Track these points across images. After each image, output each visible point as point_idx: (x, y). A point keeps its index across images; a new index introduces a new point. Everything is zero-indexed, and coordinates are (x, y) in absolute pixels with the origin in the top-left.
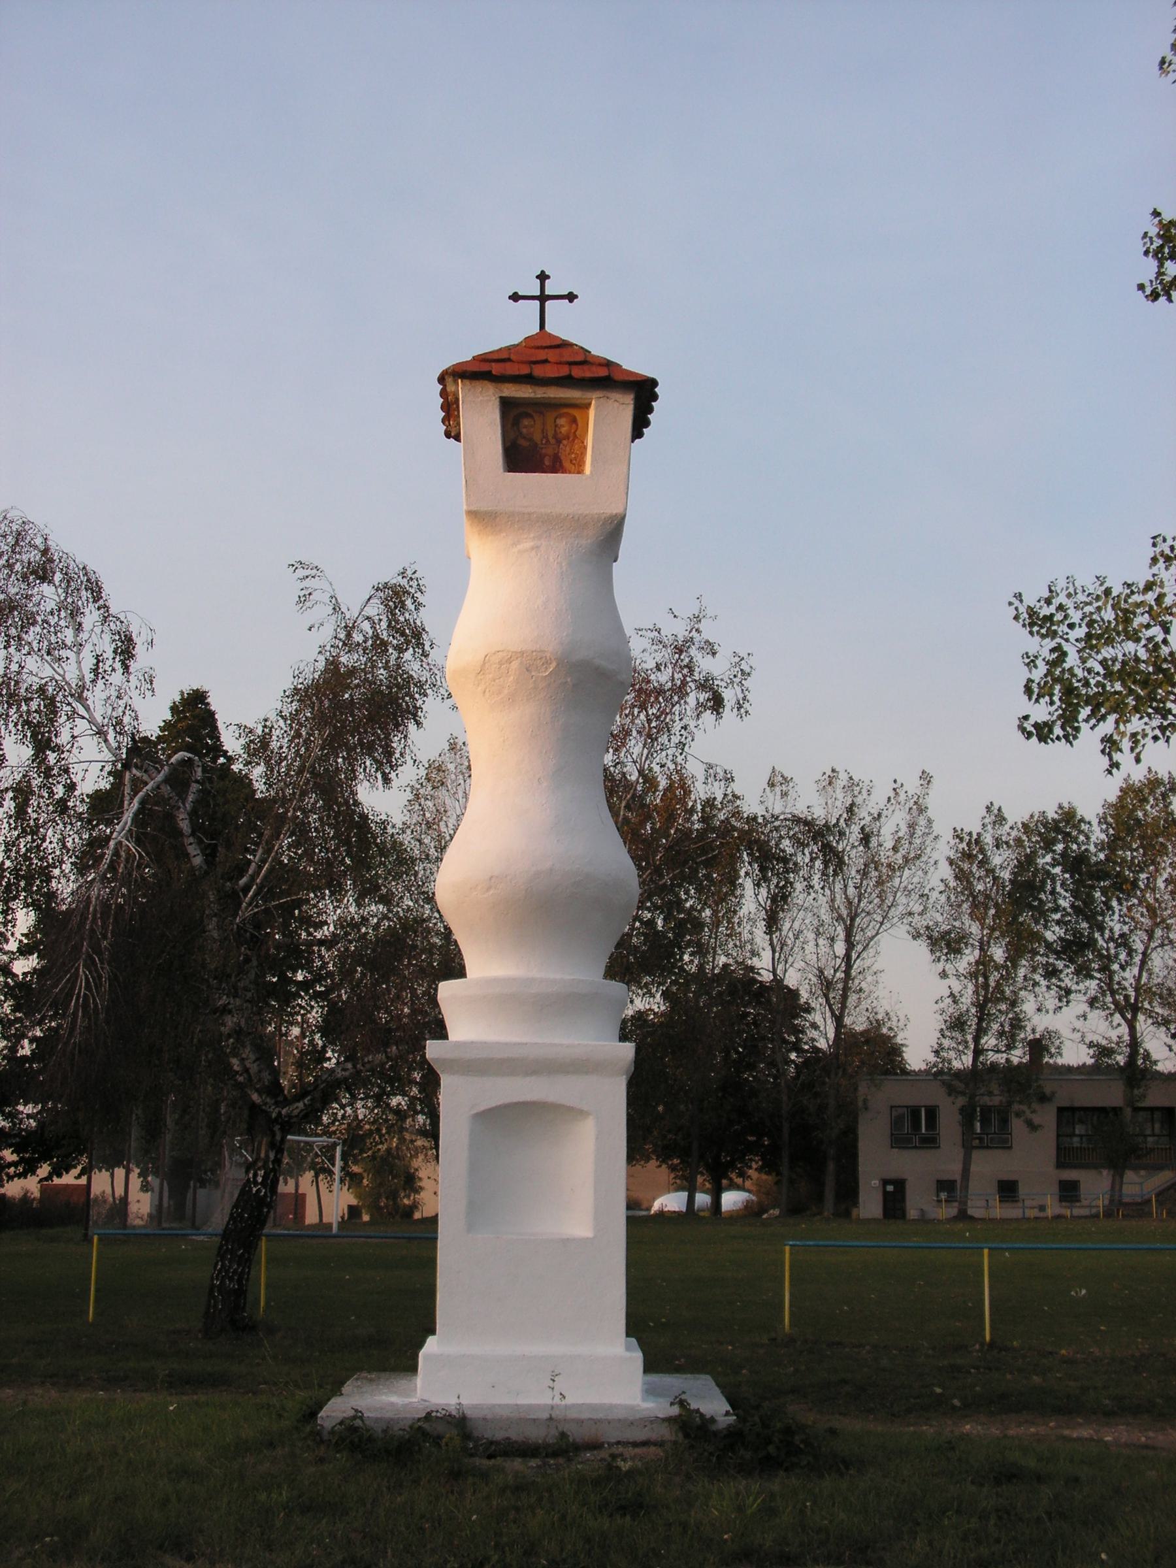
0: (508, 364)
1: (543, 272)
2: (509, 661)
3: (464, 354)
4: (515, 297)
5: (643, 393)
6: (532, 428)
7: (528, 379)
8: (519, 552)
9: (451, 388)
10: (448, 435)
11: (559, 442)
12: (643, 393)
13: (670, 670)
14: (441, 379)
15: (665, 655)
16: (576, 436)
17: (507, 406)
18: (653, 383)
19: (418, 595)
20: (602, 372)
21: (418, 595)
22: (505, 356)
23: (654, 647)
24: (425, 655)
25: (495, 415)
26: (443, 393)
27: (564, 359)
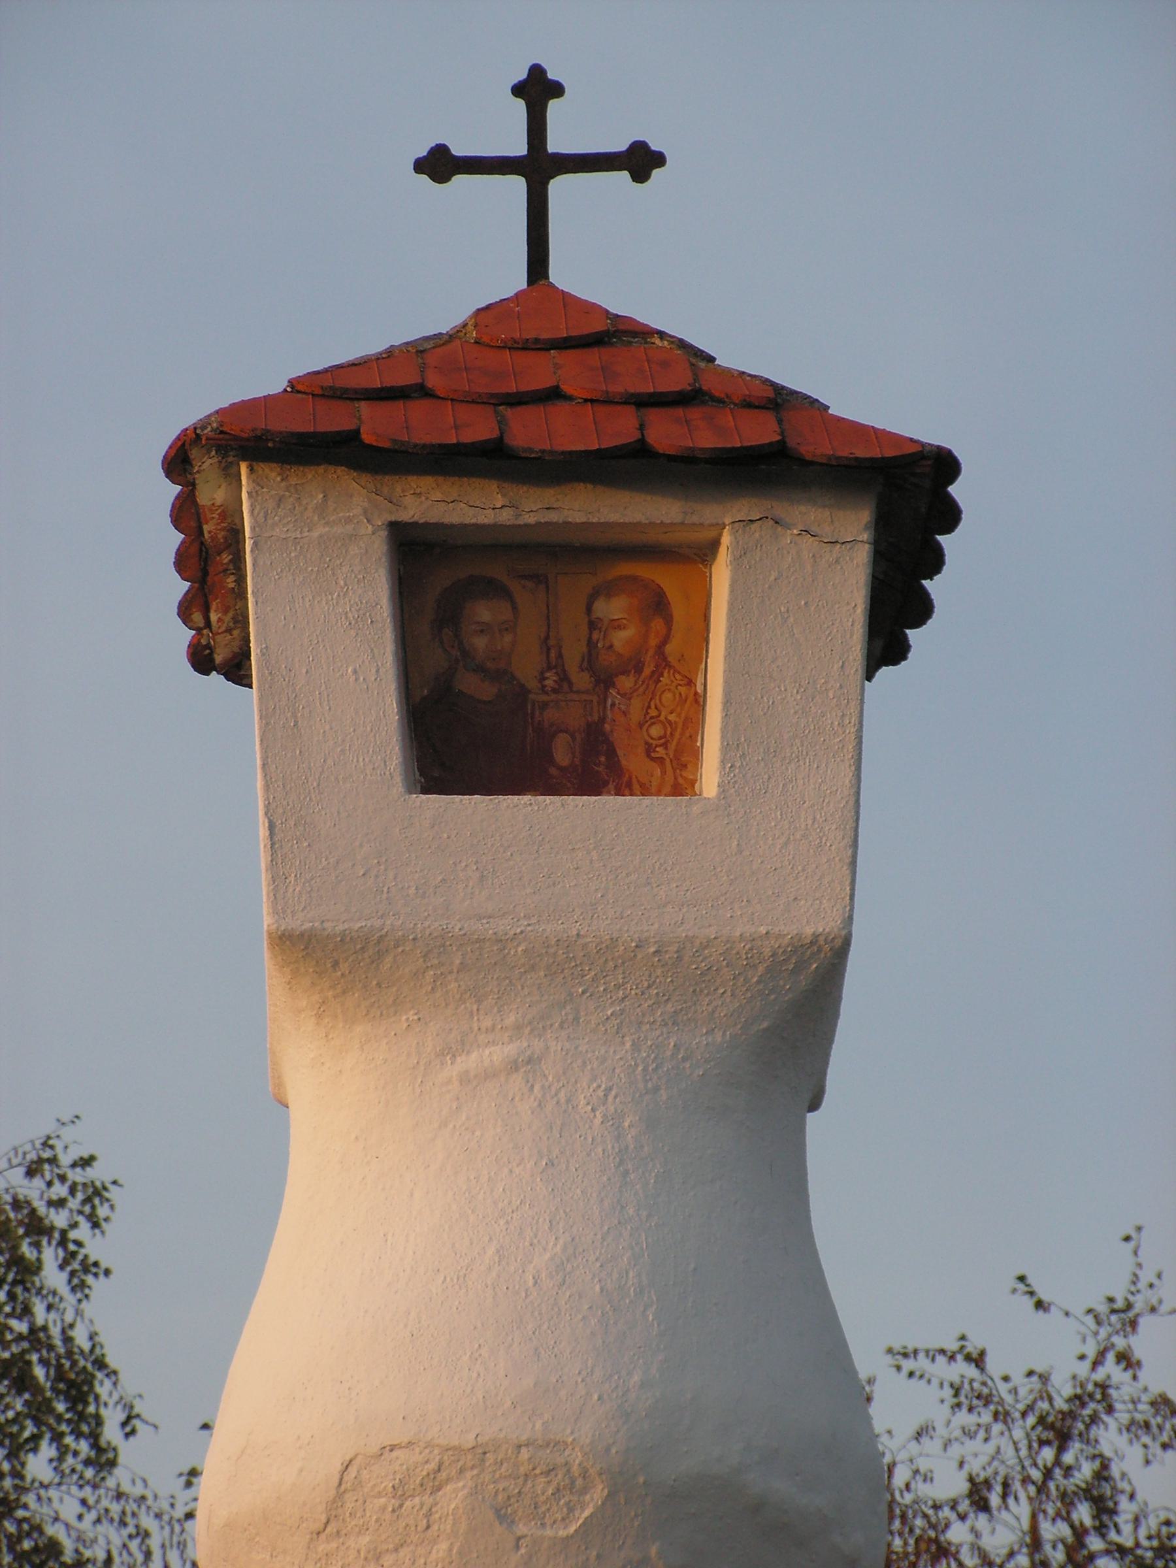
0: (418, 409)
1: (537, 72)
2: (434, 1483)
3: (258, 369)
4: (439, 164)
5: (907, 504)
6: (506, 633)
7: (493, 460)
8: (464, 1079)
9: (211, 493)
10: (201, 660)
11: (605, 682)
12: (907, 504)
13: (1022, 1510)
14: (178, 463)
15: (1003, 1449)
16: (668, 662)
17: (415, 554)
18: (945, 465)
19: (83, 1232)
20: (759, 431)
21: (83, 1232)
22: (404, 377)
23: (963, 1418)
24: (103, 1460)
25: (375, 591)
26: (185, 513)
27: (618, 388)
